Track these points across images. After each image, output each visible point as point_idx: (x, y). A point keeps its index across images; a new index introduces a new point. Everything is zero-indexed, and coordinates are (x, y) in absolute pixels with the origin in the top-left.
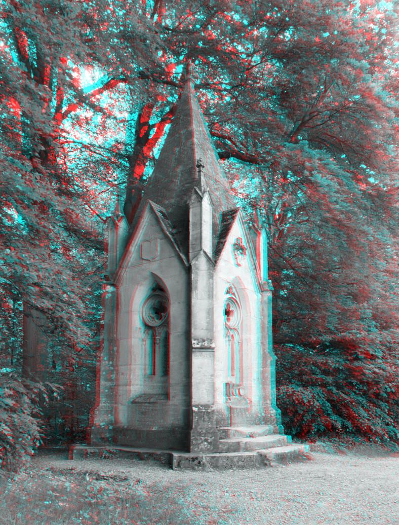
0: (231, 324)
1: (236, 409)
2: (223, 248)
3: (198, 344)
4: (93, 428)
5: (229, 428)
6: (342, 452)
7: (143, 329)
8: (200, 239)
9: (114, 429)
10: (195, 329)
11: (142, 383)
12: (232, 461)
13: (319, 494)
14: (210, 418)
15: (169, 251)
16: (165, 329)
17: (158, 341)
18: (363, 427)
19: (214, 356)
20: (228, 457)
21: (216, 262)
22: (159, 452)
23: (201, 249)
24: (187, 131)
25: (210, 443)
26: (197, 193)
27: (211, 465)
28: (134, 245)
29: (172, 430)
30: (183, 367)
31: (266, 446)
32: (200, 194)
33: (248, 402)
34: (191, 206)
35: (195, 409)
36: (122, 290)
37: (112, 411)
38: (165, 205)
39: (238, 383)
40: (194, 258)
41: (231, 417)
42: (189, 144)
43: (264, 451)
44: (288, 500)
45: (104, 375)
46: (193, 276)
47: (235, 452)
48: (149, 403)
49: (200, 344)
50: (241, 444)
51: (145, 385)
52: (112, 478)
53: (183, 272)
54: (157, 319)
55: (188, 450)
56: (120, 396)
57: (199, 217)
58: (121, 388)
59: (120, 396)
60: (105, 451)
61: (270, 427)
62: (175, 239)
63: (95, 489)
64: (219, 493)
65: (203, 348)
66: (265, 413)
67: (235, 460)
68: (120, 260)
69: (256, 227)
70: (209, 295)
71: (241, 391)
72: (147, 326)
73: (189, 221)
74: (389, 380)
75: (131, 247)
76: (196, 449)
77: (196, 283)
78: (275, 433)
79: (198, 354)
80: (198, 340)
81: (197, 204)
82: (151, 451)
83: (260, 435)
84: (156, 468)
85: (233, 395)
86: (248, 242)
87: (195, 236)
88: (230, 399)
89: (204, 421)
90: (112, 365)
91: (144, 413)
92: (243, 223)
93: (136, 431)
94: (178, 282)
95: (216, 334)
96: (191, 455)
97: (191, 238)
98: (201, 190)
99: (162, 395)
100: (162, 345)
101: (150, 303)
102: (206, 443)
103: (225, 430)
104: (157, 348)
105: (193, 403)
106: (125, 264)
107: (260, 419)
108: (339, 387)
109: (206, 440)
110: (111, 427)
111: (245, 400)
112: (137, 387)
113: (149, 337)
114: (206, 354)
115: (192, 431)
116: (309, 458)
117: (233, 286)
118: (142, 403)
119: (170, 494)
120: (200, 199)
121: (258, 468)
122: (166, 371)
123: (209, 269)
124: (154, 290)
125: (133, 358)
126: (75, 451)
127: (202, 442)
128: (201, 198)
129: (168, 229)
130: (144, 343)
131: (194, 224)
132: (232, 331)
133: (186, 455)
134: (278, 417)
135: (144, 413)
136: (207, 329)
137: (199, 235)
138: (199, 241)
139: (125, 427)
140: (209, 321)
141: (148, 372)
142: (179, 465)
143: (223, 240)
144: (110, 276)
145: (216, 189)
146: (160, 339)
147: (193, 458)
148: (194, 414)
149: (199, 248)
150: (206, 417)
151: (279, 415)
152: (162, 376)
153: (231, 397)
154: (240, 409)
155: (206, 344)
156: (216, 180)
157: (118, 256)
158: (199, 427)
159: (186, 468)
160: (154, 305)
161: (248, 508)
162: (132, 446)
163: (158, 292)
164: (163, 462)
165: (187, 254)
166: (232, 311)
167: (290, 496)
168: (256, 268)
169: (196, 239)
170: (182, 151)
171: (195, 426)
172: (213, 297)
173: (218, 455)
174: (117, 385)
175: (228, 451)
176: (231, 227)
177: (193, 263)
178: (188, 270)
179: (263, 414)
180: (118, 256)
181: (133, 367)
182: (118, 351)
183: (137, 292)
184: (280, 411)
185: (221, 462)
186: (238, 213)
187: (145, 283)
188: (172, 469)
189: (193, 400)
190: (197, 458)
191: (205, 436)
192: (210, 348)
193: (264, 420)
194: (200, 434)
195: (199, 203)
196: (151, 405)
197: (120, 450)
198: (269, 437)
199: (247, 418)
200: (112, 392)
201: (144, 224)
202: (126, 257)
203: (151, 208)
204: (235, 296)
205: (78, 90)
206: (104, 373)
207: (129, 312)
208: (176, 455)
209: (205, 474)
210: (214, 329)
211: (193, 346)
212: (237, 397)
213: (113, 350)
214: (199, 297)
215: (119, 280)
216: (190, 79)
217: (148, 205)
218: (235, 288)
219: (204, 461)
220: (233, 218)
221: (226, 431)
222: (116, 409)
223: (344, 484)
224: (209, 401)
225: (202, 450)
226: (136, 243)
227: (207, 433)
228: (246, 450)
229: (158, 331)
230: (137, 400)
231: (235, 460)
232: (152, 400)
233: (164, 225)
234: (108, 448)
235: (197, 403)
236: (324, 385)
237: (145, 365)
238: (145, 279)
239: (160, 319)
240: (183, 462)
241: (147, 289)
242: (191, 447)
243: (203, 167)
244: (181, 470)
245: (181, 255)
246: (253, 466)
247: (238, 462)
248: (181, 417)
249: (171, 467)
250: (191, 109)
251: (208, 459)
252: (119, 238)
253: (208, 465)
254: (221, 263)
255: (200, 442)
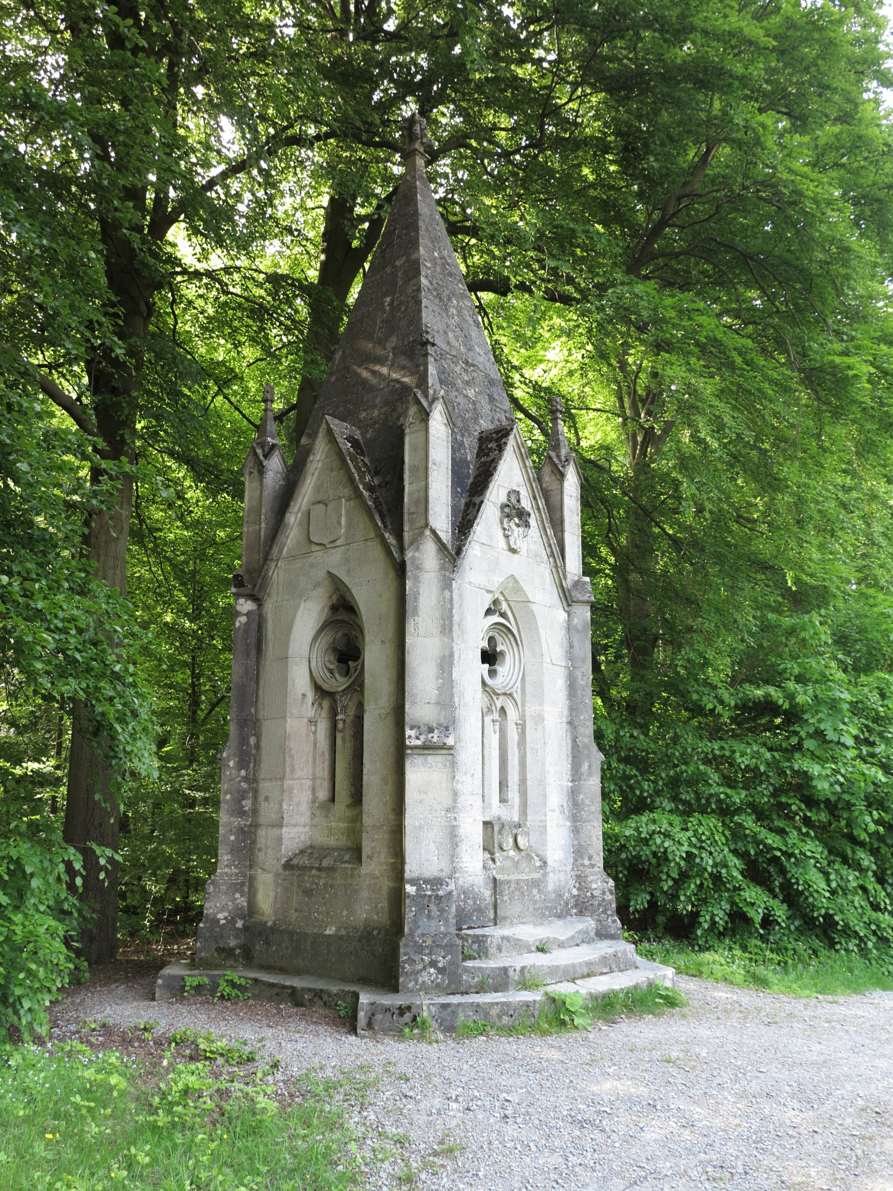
0: (497, 683)
1: (509, 882)
2: (475, 518)
3: (417, 738)
4: (201, 925)
5: (486, 931)
6: (761, 982)
7: (310, 695)
8: (424, 501)
9: (246, 928)
10: (414, 703)
11: (308, 821)
12: (487, 1015)
13: (655, 1106)
14: (442, 911)
15: (362, 525)
16: (355, 700)
17: (340, 725)
18: (817, 918)
19: (454, 764)
20: (478, 1005)
21: (459, 551)
22: (334, 989)
23: (427, 525)
24: (408, 260)
25: (441, 971)
26: (418, 402)
27: (441, 1024)
28: (296, 509)
29: (366, 935)
30: (390, 788)
31: (572, 975)
32: (425, 404)
33: (538, 864)
34: (407, 431)
35: (410, 889)
36: (269, 607)
37: (242, 884)
38: (360, 421)
39: (516, 819)
40: (411, 544)
41: (496, 902)
42: (410, 290)
43: (563, 989)
44: (582, 1124)
45: (227, 802)
46: (409, 584)
47: (496, 991)
48: (319, 869)
49: (422, 738)
50: (511, 972)
51: (313, 826)
52: (222, 1055)
53: (392, 574)
54: (341, 675)
55: (395, 988)
56: (260, 850)
57: (423, 453)
58: (262, 832)
59: (260, 850)
60: (222, 982)
61: (589, 924)
62: (376, 501)
63: (175, 1089)
64: (437, 1102)
65: (428, 748)
66: (579, 889)
67: (494, 1012)
68: (265, 542)
69: (556, 460)
70: (443, 627)
71: (519, 838)
72: (320, 692)
73: (403, 462)
74: (875, 802)
75: (287, 515)
76: (411, 985)
77: (416, 599)
78: (602, 934)
79: (418, 760)
80: (419, 727)
81: (418, 426)
82: (319, 985)
83: (561, 945)
84: (321, 1029)
85: (502, 849)
86: (535, 498)
87: (416, 495)
88: (493, 860)
89: (429, 917)
90: (245, 779)
91: (308, 893)
92: (523, 458)
93: (291, 934)
94: (380, 596)
95: (461, 713)
96: (398, 1000)
97: (406, 500)
98: (426, 396)
99: (349, 849)
100: (349, 733)
101: (326, 639)
102: (432, 970)
103: (477, 936)
104: (339, 741)
105: (407, 875)
106: (275, 551)
107: (567, 904)
108: (761, 815)
109: (433, 964)
110: (239, 924)
111: (529, 857)
112: (296, 830)
113: (324, 713)
114: (435, 760)
115: (402, 942)
116: (671, 1002)
117: (501, 598)
118: (304, 868)
119: (334, 1104)
120: (425, 416)
121: (544, 1033)
122: (357, 798)
123: (442, 568)
124: (334, 608)
125: (287, 764)
126: (160, 981)
127: (425, 968)
128: (428, 415)
129: (362, 478)
130: (313, 728)
131: (414, 469)
132: (501, 698)
133: (387, 1000)
134: (609, 897)
135: (308, 893)
136: (438, 703)
137: (422, 494)
138: (422, 506)
139: (269, 924)
140: (443, 684)
141: (323, 794)
142: (370, 1025)
143: (477, 500)
144: (246, 577)
145: (467, 383)
146: (344, 721)
147: (400, 1008)
148: (407, 901)
149: (423, 523)
150: (433, 907)
151: (611, 893)
152: (348, 806)
153: (497, 855)
154: (518, 882)
155: (435, 737)
156: (467, 363)
157: (263, 533)
158: (419, 932)
159: (385, 1032)
160: (334, 642)
161: (490, 1143)
162: (282, 971)
163: (342, 616)
164: (342, 1013)
165: (399, 535)
166: (502, 653)
167: (590, 1114)
168: (558, 551)
169: (417, 503)
170: (396, 303)
171: (410, 929)
172: (451, 630)
173: (455, 1000)
174: (255, 826)
175: (480, 989)
176: (495, 468)
177: (409, 555)
178: (400, 570)
179: (575, 892)
180: (263, 533)
181: (288, 783)
182: (258, 746)
183: (299, 614)
184: (611, 883)
185: (461, 1017)
186: (511, 437)
187: (314, 594)
188: (356, 1034)
189: (407, 868)
190: (409, 1008)
191: (430, 954)
192: (444, 747)
193: (576, 906)
194: (420, 950)
195: (423, 424)
196: (323, 874)
197: (256, 981)
198: (584, 948)
199: (535, 902)
200: (244, 841)
201: (315, 465)
202: (278, 537)
203: (330, 431)
204: (509, 622)
205: (260, 25)
206: (228, 797)
207: (284, 659)
208: (365, 999)
209: (424, 1046)
210: (456, 700)
211: (407, 743)
212: (512, 853)
213: (248, 744)
214: (422, 630)
215: (264, 587)
216: (416, 150)
217: (324, 426)
218: (506, 600)
219: (425, 1014)
220: (501, 449)
221: (480, 940)
222: (252, 879)
223: (718, 1080)
224: (442, 870)
225: (424, 988)
226: (298, 505)
227: (436, 945)
228: (524, 985)
229: (342, 701)
230: (295, 862)
231: (494, 1012)
232: (325, 863)
233: (353, 470)
234: (231, 975)
235: (415, 875)
236: (725, 811)
237: (314, 779)
238: (316, 586)
239: (347, 673)
240: (379, 1017)
241: (322, 610)
242: (401, 980)
243: (433, 345)
244: (374, 1037)
245: (387, 535)
246: (534, 1029)
247: (500, 1017)
248: (384, 904)
249: (353, 1030)
250: (416, 214)
251: (433, 1009)
252: (266, 493)
253: (435, 1025)
254: (473, 551)
255: (420, 967)
